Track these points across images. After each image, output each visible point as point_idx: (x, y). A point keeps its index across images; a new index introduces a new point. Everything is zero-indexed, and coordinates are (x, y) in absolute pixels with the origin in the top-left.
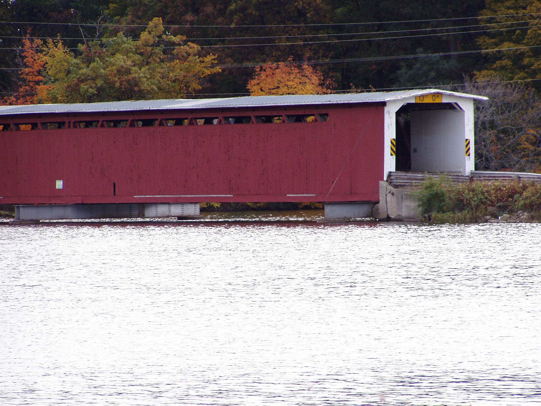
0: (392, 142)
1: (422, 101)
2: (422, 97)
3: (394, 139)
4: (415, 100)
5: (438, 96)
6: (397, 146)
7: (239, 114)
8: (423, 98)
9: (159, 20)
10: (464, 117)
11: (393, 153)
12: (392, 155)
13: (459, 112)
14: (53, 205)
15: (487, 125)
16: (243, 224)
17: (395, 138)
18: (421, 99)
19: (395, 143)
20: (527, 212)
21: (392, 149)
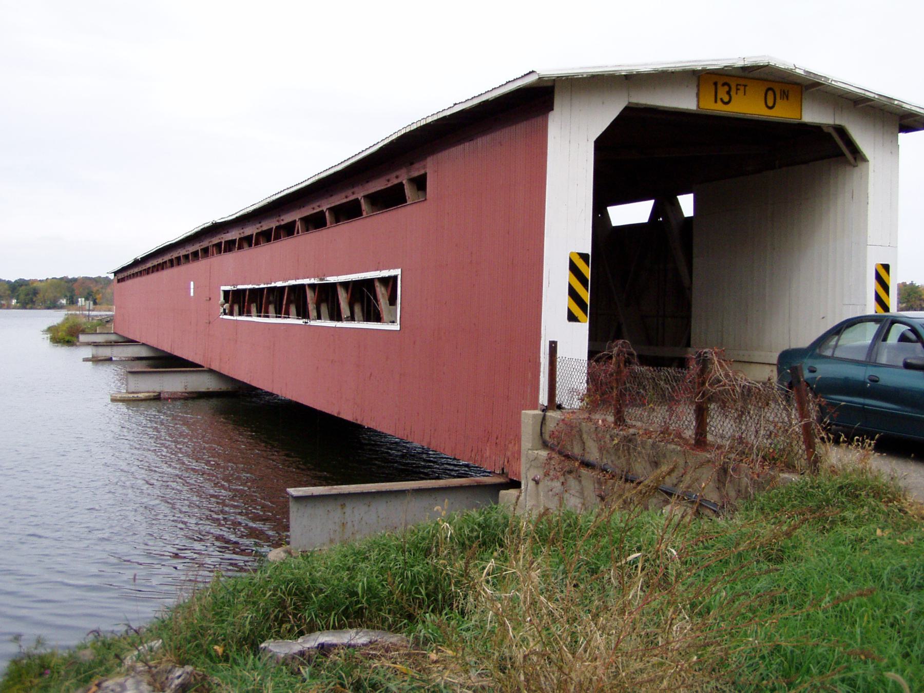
0: (573, 268)
1: (727, 103)
2: (726, 88)
3: (584, 256)
4: (695, 100)
5: (785, 95)
6: (598, 286)
7: (278, 221)
8: (729, 93)
9: (772, 371)
10: (867, 183)
11: (577, 311)
12: (572, 317)
13: (848, 163)
14: (113, 344)
15: (175, 262)
16: (681, 62)
17: (588, 250)
18: (719, 97)
19: (587, 272)
20: (817, 379)
21: (572, 293)
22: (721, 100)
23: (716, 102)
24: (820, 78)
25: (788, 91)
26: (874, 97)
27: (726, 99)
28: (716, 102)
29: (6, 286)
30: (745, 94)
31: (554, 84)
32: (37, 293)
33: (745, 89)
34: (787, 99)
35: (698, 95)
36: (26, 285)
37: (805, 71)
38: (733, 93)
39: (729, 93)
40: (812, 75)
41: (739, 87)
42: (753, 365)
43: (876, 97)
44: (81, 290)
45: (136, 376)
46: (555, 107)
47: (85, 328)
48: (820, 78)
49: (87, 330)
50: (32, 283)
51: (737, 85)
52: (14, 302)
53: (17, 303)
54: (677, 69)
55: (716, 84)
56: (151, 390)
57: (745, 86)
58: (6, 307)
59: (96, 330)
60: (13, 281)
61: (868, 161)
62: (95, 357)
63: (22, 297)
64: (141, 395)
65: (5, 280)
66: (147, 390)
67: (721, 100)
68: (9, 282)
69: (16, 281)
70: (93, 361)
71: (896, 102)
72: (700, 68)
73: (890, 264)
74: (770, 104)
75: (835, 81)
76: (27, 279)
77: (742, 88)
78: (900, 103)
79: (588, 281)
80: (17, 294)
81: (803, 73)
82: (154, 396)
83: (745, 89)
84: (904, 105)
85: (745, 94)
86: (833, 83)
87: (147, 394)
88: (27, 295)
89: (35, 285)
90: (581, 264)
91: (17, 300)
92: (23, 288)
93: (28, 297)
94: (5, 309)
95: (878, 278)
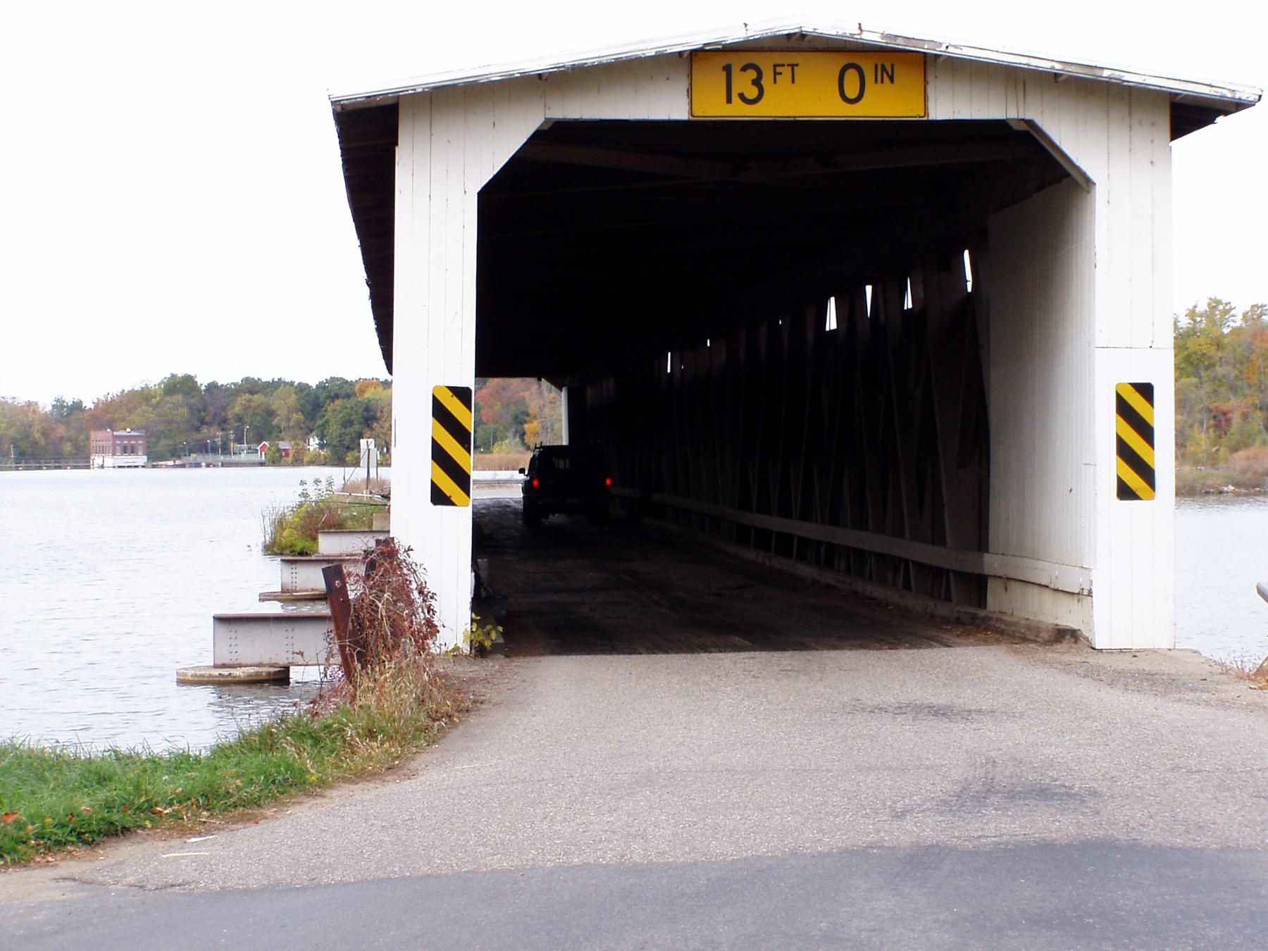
0: (440, 413)
2: (752, 74)
4: (686, 101)
8: (757, 82)
12: (439, 497)
22: (741, 96)
23: (729, 101)
24: (920, 44)
25: (892, 66)
26: (1053, 68)
27: (752, 93)
28: (729, 101)
29: (292, 400)
30: (793, 81)
31: (398, 101)
32: (375, 418)
33: (793, 70)
34: (892, 79)
35: (690, 92)
36: (348, 396)
37: (883, 36)
38: (767, 81)
39: (757, 82)
40: (900, 41)
41: (778, 70)
42: (1031, 587)
43: (1058, 66)
44: (498, 407)
45: (234, 627)
46: (399, 143)
47: (345, 520)
48: (922, 43)
49: (349, 523)
50: (362, 392)
51: (775, 66)
52: (314, 443)
53: (322, 446)
54: (604, 60)
55: (728, 69)
56: (266, 660)
57: (793, 66)
58: (290, 459)
59: (371, 526)
60: (313, 384)
61: (1095, 184)
62: (288, 591)
63: (334, 429)
64: (238, 672)
65: (292, 383)
66: (256, 661)
67: (741, 96)
68: (303, 388)
69: (321, 386)
70: (280, 601)
71: (1106, 73)
72: (653, 54)
73: (1153, 383)
74: (852, 92)
75: (955, 47)
76: (351, 377)
77: (786, 71)
78: (1117, 73)
79: (470, 434)
80: (320, 422)
81: (880, 40)
82: (269, 673)
83: (793, 70)
84: (1127, 77)
85: (793, 81)
86: (950, 49)
87: (252, 670)
88: (348, 423)
89: (367, 395)
90: (454, 406)
91: (321, 439)
92: (338, 402)
93: (348, 430)
94: (287, 465)
95: (1124, 409)
